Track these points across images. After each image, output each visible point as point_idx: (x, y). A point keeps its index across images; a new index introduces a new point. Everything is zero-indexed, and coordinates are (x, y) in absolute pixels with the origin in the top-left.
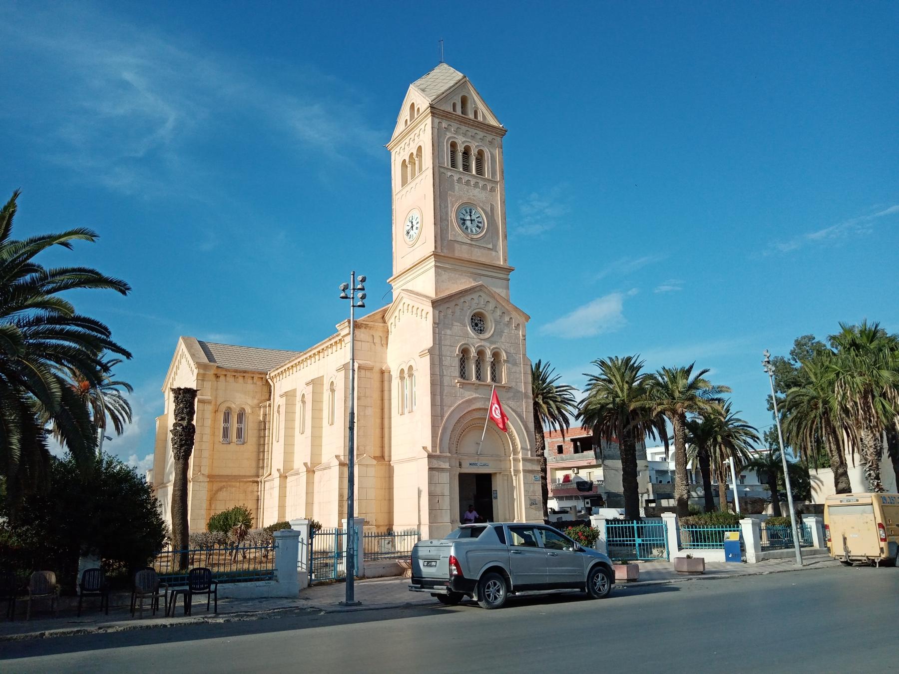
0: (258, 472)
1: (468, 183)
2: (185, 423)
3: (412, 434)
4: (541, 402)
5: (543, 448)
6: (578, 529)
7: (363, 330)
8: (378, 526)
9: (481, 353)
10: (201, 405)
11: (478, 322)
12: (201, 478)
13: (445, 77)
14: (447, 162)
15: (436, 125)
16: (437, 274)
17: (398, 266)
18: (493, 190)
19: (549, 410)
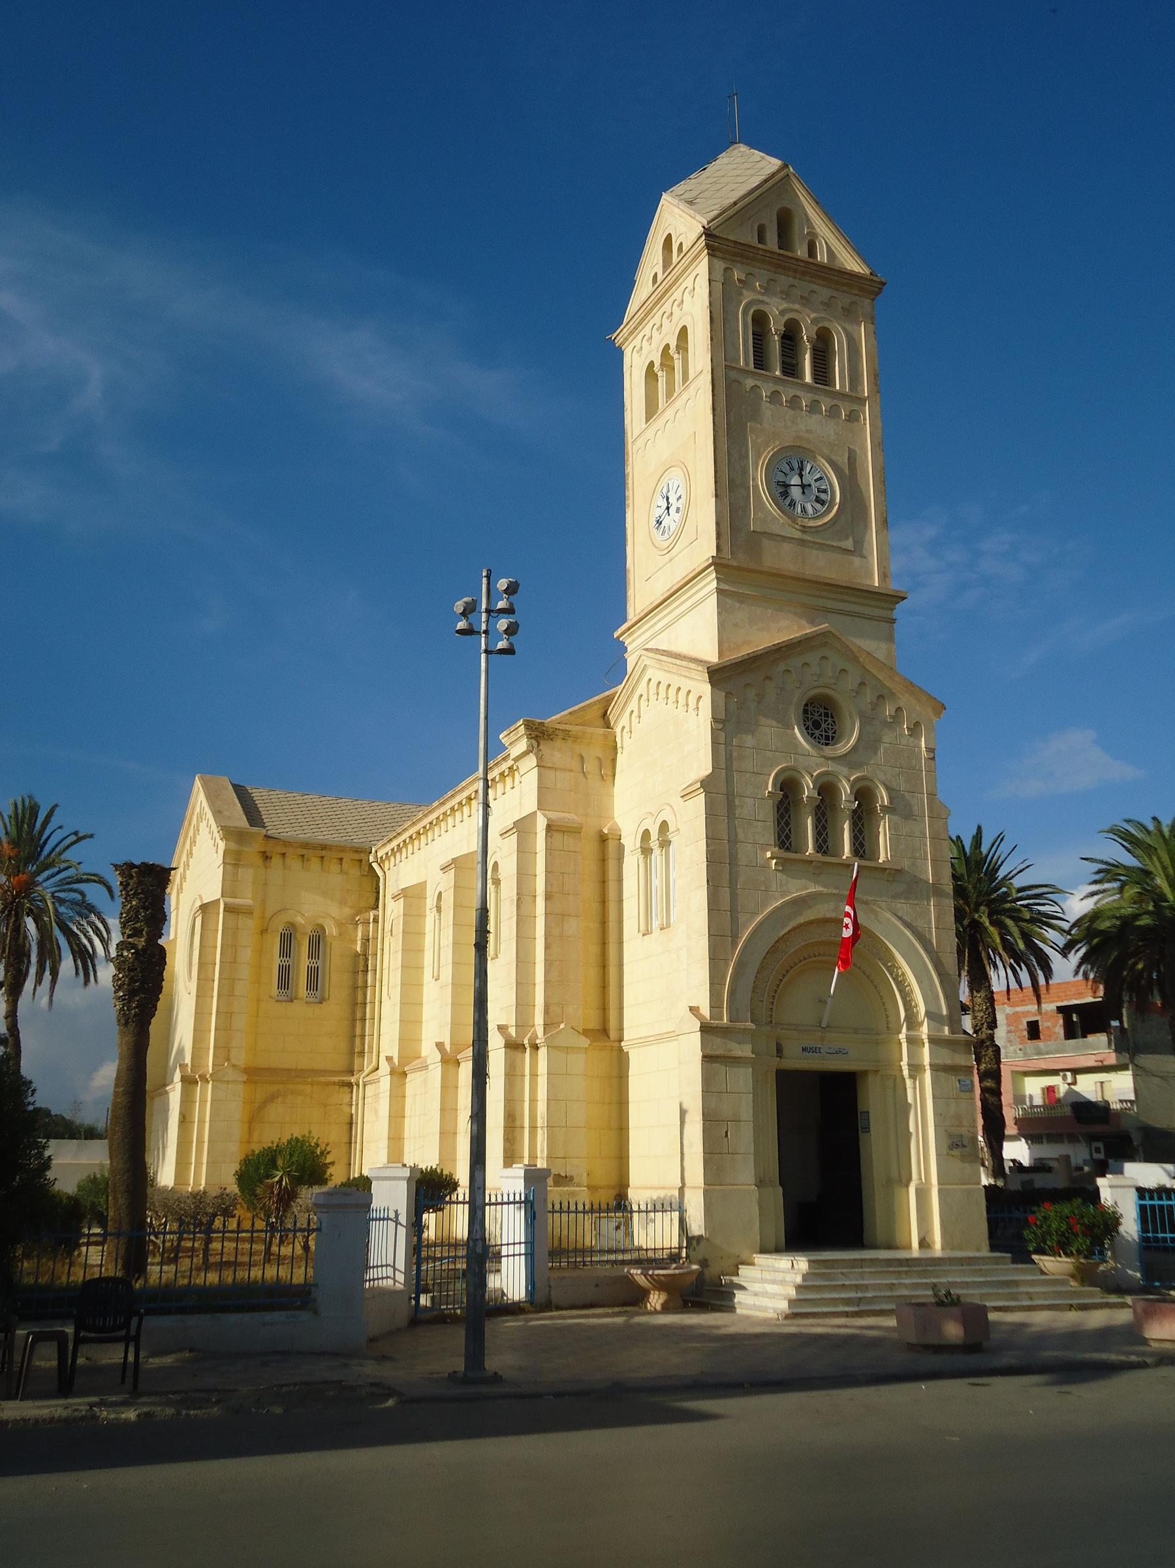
0: (352, 1063)
1: (794, 402)
2: (141, 942)
3: (668, 977)
4: (986, 921)
5: (993, 1024)
6: (1066, 1209)
7: (558, 743)
8: (592, 1188)
9: (827, 790)
10: (231, 916)
11: (821, 719)
12: (231, 1075)
13: (742, 170)
14: (744, 357)
15: (719, 276)
16: (720, 604)
17: (639, 598)
18: (853, 417)
19: (1003, 940)
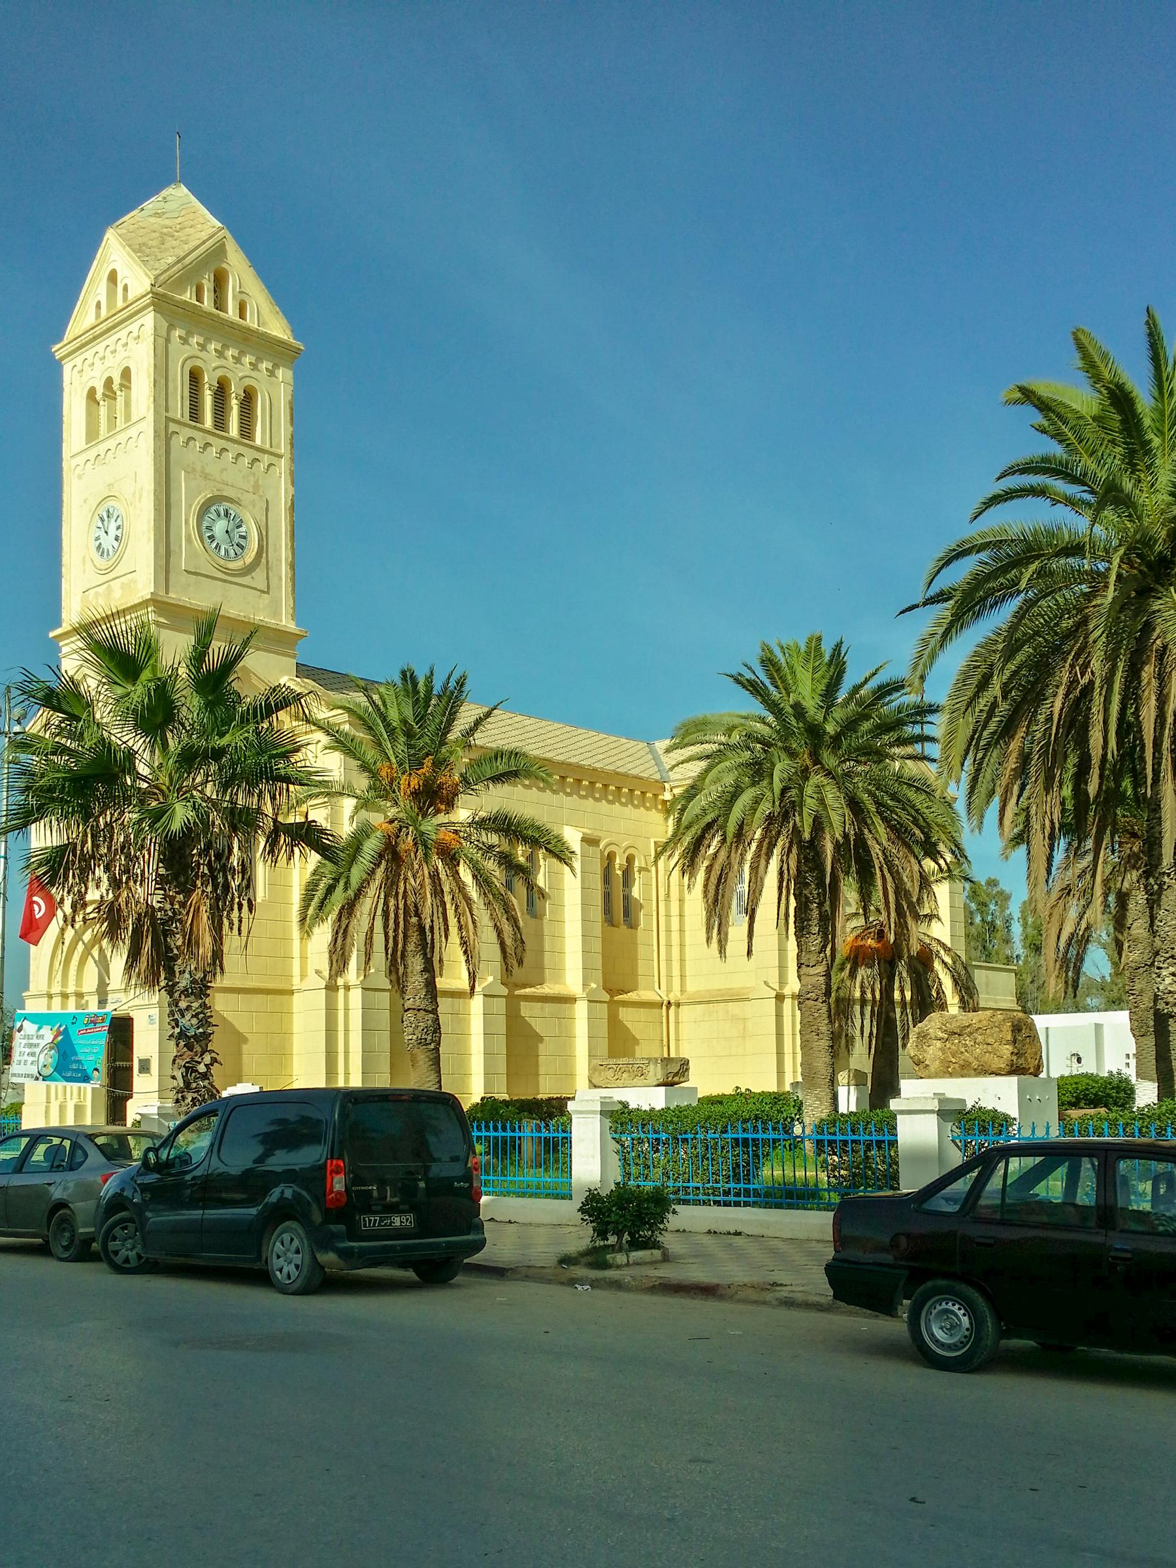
13: (181, 217)
14: (179, 409)
